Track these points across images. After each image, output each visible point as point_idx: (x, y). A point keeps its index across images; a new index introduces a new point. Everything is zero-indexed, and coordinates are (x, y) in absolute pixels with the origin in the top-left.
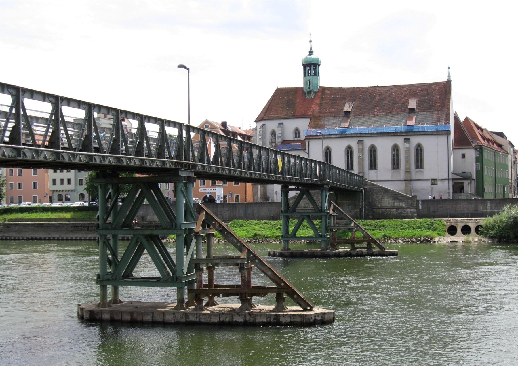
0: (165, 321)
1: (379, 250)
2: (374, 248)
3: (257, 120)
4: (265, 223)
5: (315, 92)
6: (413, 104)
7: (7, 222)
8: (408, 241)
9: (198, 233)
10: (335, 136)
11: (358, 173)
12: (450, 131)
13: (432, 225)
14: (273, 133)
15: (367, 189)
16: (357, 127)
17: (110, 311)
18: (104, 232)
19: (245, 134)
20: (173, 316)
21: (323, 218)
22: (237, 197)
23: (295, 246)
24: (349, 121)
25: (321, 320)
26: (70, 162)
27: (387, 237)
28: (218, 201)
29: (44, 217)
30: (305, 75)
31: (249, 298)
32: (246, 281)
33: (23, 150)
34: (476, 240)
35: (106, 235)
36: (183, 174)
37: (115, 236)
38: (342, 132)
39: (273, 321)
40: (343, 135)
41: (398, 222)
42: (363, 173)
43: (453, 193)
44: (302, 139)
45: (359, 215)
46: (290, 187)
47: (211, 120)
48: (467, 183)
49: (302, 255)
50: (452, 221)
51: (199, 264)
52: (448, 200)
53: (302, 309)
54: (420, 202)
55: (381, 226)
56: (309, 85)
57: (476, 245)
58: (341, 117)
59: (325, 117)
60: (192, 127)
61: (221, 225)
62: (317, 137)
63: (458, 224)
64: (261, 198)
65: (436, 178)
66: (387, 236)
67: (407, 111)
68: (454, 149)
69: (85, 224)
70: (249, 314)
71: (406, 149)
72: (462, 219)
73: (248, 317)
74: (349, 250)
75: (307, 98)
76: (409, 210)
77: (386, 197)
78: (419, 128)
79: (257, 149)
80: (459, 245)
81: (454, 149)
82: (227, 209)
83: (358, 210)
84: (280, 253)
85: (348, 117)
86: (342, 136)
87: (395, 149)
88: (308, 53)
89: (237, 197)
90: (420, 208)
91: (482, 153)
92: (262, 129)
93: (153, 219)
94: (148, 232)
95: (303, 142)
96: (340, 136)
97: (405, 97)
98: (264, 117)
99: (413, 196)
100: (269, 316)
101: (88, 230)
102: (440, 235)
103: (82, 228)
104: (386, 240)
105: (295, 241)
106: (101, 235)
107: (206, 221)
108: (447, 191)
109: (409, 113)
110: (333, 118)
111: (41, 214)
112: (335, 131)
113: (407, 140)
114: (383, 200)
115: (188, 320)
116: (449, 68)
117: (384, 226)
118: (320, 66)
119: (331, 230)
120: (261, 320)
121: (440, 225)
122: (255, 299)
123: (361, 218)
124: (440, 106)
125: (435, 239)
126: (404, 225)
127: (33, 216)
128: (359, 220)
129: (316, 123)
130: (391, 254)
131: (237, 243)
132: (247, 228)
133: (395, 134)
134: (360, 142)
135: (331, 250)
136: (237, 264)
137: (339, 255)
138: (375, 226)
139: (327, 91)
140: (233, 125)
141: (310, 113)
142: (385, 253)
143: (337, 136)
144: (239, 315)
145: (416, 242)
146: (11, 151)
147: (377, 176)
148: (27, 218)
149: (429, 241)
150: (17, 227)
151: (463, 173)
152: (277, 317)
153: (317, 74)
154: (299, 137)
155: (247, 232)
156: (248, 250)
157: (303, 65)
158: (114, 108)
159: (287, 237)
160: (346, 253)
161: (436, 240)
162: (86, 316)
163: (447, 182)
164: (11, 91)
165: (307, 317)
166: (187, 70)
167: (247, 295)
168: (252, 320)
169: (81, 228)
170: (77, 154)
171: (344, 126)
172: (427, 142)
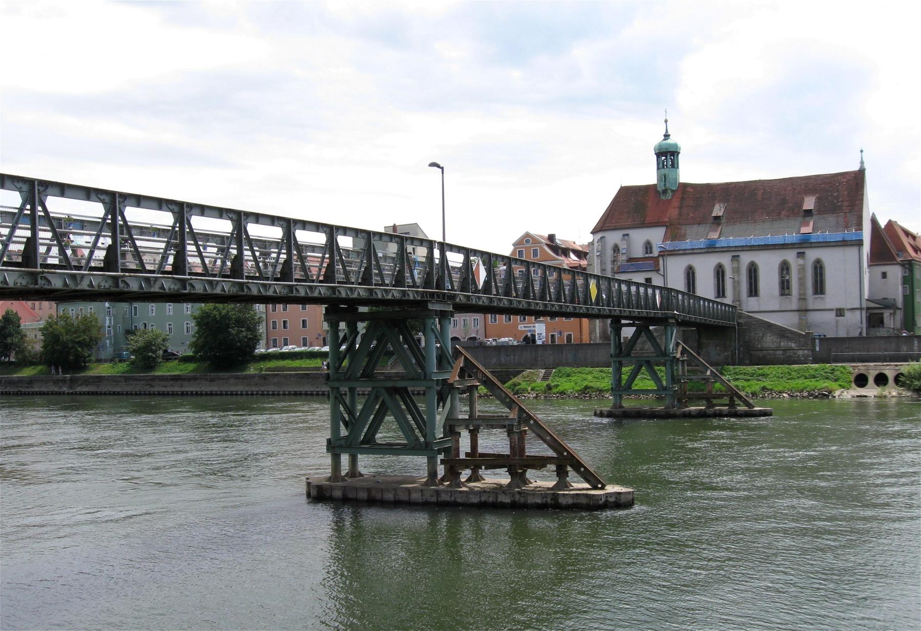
0: (411, 501)
1: (746, 408)
2: (739, 405)
3: (595, 230)
4: (601, 371)
5: (673, 191)
6: (809, 203)
7: (263, 372)
8: (797, 396)
9: (452, 384)
10: (700, 251)
11: (733, 301)
12: (862, 240)
13: (832, 373)
14: (616, 249)
15: (741, 323)
16: (731, 238)
17: (342, 487)
18: (336, 384)
19: (581, 249)
20: (420, 494)
21: (668, 364)
22: (569, 337)
23: (629, 403)
24: (720, 229)
25: (615, 502)
26: (260, 294)
27: (768, 390)
28: (539, 342)
29: (312, 366)
30: (658, 169)
31: (520, 471)
32: (518, 448)
33: (191, 281)
34: (894, 394)
35: (338, 388)
36: (434, 307)
37: (352, 390)
38: (802, 240)
39: (550, 502)
40: (711, 249)
41: (784, 369)
42: (739, 301)
43: (867, 328)
46: (623, 322)
47: (535, 231)
48: (888, 314)
49: (639, 415)
50: (861, 367)
51: (454, 425)
52: (860, 338)
53: (590, 487)
54: (817, 341)
55: (760, 375)
57: (894, 400)
58: (708, 225)
59: (686, 225)
60: (448, 244)
61: (485, 374)
62: (675, 253)
63: (870, 371)
64: (601, 337)
65: (842, 307)
66: (767, 389)
67: (802, 214)
68: (871, 265)
70: (519, 492)
71: (799, 267)
72: (875, 365)
73: (517, 497)
74: (704, 408)
76: (800, 352)
77: (769, 334)
78: (817, 236)
79: (569, 274)
80: (872, 401)
81: (869, 266)
83: (730, 353)
84: (609, 411)
85: (719, 224)
86: (710, 250)
87: (785, 267)
88: (663, 137)
89: (569, 337)
90: (818, 349)
91: (911, 271)
92: (600, 243)
94: (390, 384)
95: (656, 260)
96: (706, 250)
97: (798, 193)
98: (602, 227)
99: (807, 333)
100: (546, 496)
102: (844, 388)
104: (766, 395)
105: (639, 396)
106: (332, 388)
107: (465, 369)
108: (859, 325)
109: (804, 216)
110: (697, 226)
111: (308, 361)
112: (701, 243)
113: (801, 255)
114: (765, 338)
115: (439, 499)
116: (862, 151)
117: (764, 375)
118: (680, 155)
119: (679, 381)
120: (534, 501)
121: (843, 374)
122: (530, 474)
123: (733, 364)
124: (849, 206)
125: (835, 393)
126: (792, 373)
127: (297, 363)
128: (729, 366)
129: (674, 233)
130: (762, 413)
131: (505, 398)
132: (576, 378)
133: (784, 246)
134: (735, 258)
135: (678, 408)
136: (505, 427)
137: (689, 416)
138: (752, 375)
139: (689, 189)
140: (562, 237)
141: (667, 220)
142: (754, 413)
143: (703, 251)
144: (506, 494)
145: (807, 397)
146: (173, 283)
148: (290, 366)
149: (825, 395)
150: (276, 379)
151: (884, 299)
152: (555, 497)
153: (676, 166)
154: (651, 252)
155: (576, 384)
156: (520, 407)
157: (655, 154)
158: (326, 224)
159: (619, 390)
160: (699, 413)
161: (837, 393)
162: (314, 493)
163: (858, 312)
164: (171, 207)
165: (594, 498)
166: (441, 170)
167: (517, 468)
168: (522, 500)
170: (270, 285)
171: (712, 237)
172: (828, 257)
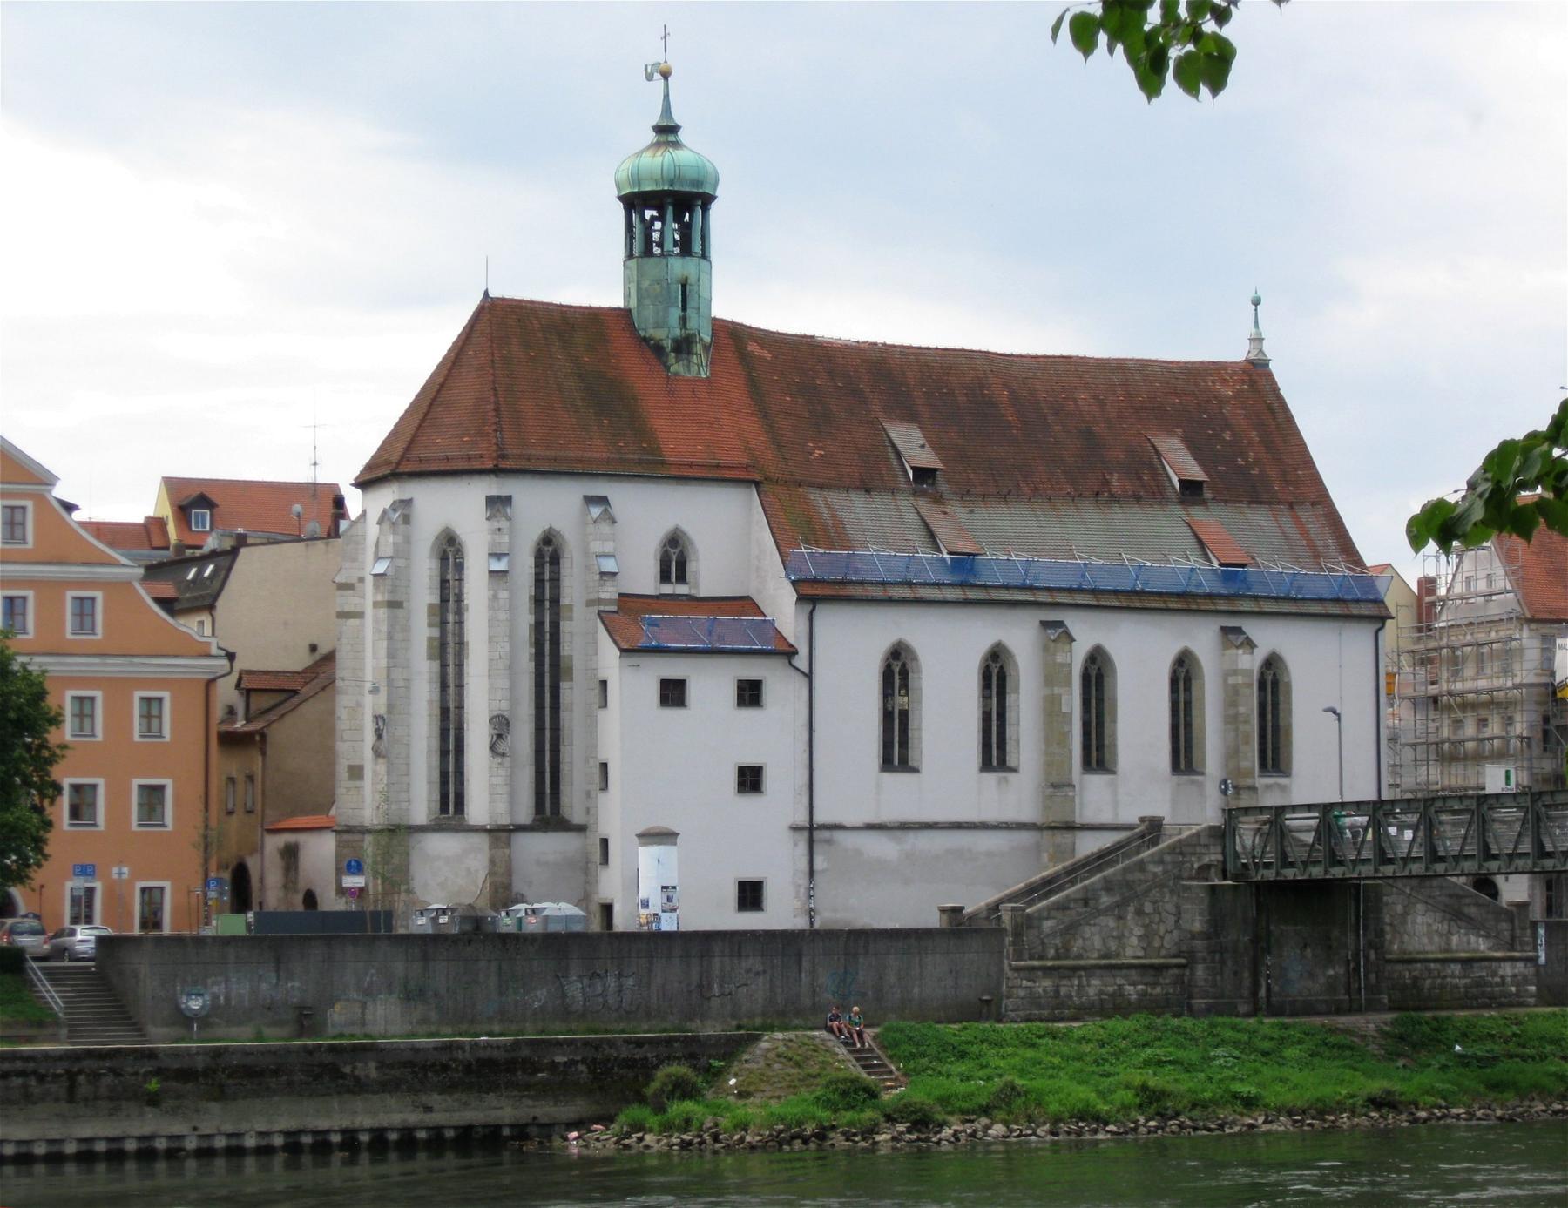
30: (630, 255)
44: (702, 594)
45: (1343, 991)
56: (684, 308)
69: (47, 1056)
75: (676, 374)
76: (1507, 970)
82: (754, 963)
83: (1341, 971)
87: (1183, 674)
93: (364, 1024)
101: (71, 1097)
103: (33, 1082)
114: (1409, 919)
116: (1256, 302)
134: (1057, 634)
147: (1116, 804)
154: (682, 578)
157: (621, 198)
169: (25, 1086)
